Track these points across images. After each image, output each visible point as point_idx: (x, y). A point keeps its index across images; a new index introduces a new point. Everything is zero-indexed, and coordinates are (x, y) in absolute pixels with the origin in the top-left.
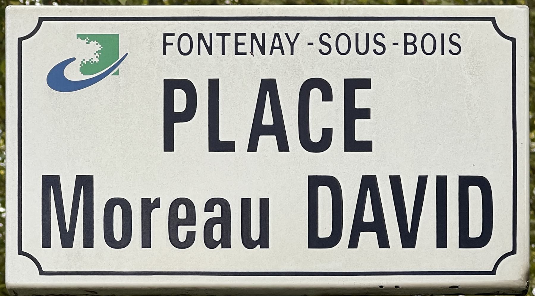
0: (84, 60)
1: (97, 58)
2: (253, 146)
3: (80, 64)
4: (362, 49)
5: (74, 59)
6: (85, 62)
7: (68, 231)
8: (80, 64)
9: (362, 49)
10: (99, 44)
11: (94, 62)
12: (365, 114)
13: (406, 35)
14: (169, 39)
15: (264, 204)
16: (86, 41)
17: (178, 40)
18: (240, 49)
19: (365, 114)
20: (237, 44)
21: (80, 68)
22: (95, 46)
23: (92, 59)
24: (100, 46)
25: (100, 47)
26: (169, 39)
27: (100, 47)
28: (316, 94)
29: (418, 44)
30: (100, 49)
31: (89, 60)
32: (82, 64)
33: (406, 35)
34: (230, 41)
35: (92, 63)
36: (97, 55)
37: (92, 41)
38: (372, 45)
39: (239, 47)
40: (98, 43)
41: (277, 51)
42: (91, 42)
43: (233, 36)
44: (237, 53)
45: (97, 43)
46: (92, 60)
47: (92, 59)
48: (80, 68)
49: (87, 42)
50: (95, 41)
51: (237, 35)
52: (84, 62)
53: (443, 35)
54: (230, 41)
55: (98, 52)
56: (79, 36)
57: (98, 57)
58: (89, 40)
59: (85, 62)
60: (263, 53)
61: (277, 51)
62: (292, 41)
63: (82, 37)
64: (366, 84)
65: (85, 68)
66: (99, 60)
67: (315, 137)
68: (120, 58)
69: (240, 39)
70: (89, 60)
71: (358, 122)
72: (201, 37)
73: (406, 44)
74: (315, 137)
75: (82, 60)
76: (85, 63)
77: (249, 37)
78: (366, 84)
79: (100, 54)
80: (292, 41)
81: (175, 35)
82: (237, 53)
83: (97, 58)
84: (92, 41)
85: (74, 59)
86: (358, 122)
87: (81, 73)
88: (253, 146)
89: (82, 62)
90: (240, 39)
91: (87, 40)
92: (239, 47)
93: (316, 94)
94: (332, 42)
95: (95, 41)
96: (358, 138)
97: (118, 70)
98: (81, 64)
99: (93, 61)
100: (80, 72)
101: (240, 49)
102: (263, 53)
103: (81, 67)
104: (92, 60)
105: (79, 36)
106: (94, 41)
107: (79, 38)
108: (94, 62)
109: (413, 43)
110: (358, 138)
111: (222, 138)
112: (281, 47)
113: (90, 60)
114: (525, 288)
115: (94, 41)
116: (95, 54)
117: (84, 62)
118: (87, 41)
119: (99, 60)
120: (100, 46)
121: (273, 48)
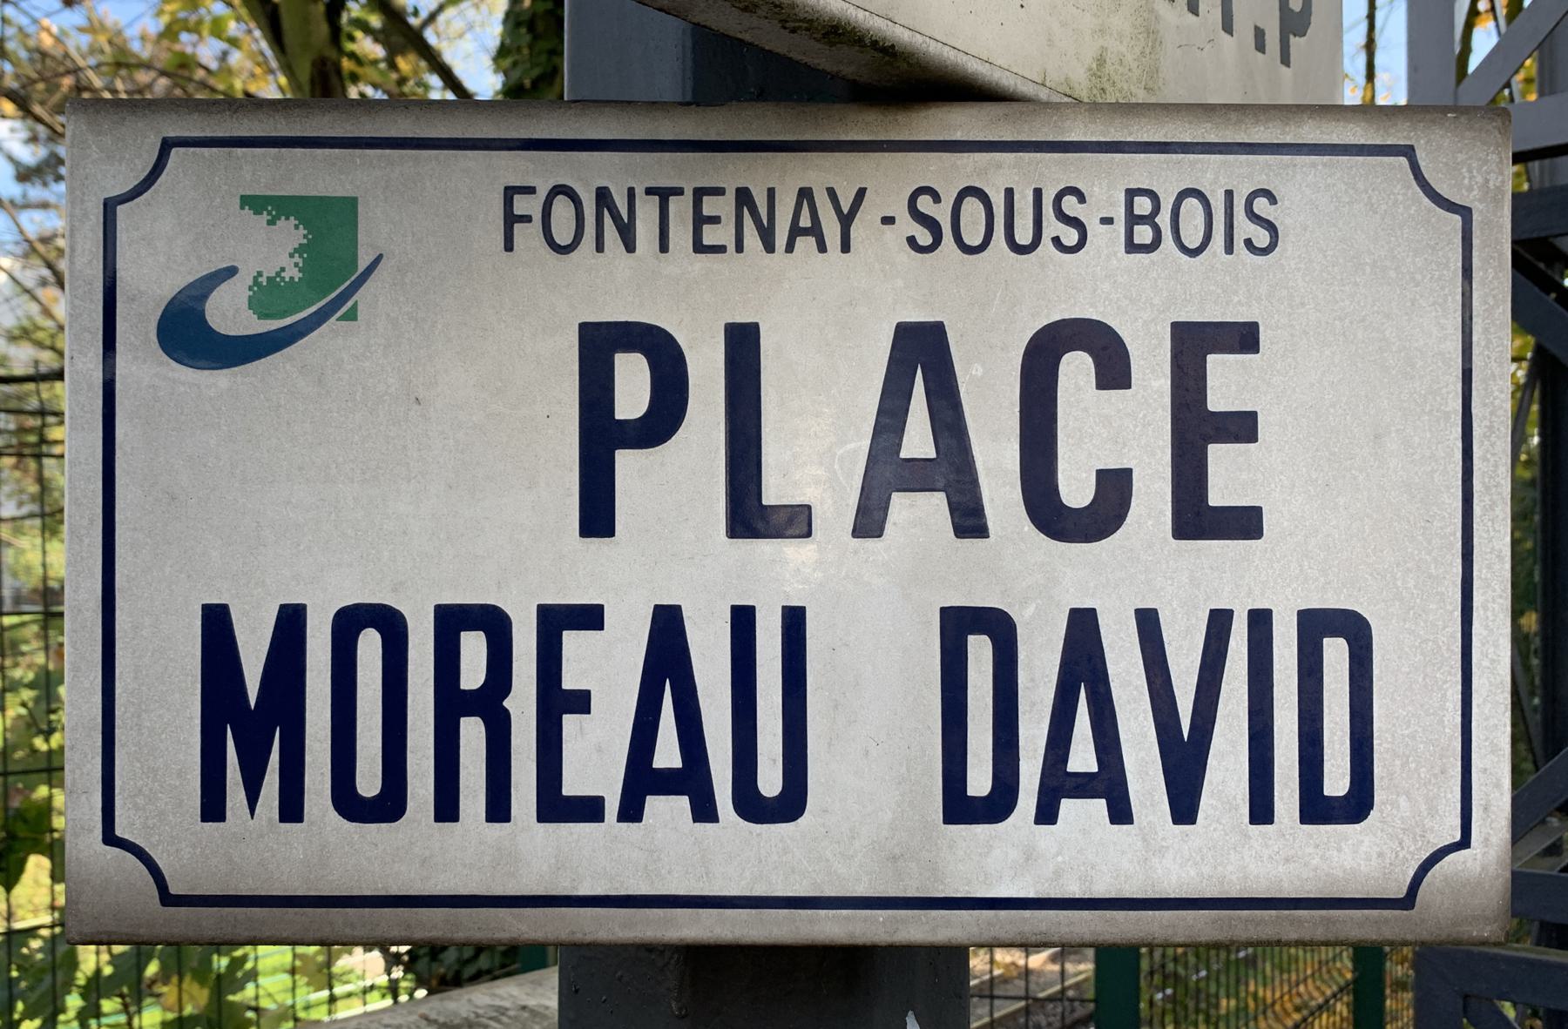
0: (260, 274)
1: (297, 269)
2: (869, 522)
3: (250, 287)
4: (1024, 236)
5: (231, 272)
6: (263, 280)
7: (253, 703)
8: (250, 287)
9: (1024, 236)
10: (301, 226)
11: (287, 279)
12: (1242, 427)
13: (1131, 194)
14: (521, 205)
15: (794, 621)
16: (265, 217)
17: (1416, 178)
18: (710, 236)
19: (1242, 427)
20: (700, 221)
21: (250, 297)
22: (290, 234)
23: (283, 269)
24: (306, 232)
25: (305, 237)
26: (521, 205)
27: (305, 237)
28: (1076, 369)
29: (1164, 220)
30: (305, 241)
31: (274, 275)
32: (254, 285)
33: (1131, 194)
34: (680, 208)
35: (282, 284)
36: (297, 259)
37: (283, 218)
38: (1052, 226)
39: (706, 228)
40: (300, 223)
41: (805, 244)
42: (279, 219)
43: (689, 194)
44: (699, 247)
45: (297, 222)
46: (283, 274)
47: (283, 269)
48: (250, 297)
49: (268, 221)
50: (292, 218)
51: (699, 193)
52: (260, 279)
53: (1229, 194)
54: (680, 208)
55: (300, 250)
56: (247, 201)
57: (301, 265)
58: (274, 213)
59: (263, 280)
60: (723, 249)
61: (805, 244)
62: (846, 211)
63: (253, 203)
64: (1244, 338)
65: (267, 295)
66: (301, 275)
67: (1076, 490)
68: (362, 265)
69: (710, 206)
70: (274, 275)
71: (1218, 455)
72: (603, 196)
73: (1133, 220)
74: (1076, 490)
75: (256, 274)
76: (265, 284)
77: (730, 196)
78: (1244, 338)
79: (305, 255)
80: (846, 211)
81: (771, 186)
82: (699, 247)
83: (297, 269)
84: (283, 218)
85: (231, 272)
86: (1218, 455)
87: (252, 311)
88: (869, 522)
89: (255, 279)
90: (710, 206)
91: (269, 213)
92: (706, 228)
93: (1076, 369)
94: (942, 214)
95: (292, 218)
96: (1217, 497)
97: (356, 302)
98: (251, 284)
99: (286, 275)
100: (250, 309)
101: (710, 236)
102: (769, 247)
103: (251, 293)
104: (283, 274)
105: (247, 201)
106: (287, 219)
107: (247, 207)
108: (287, 279)
109: (1150, 220)
110: (1217, 497)
111: (772, 494)
112: (816, 231)
113: (278, 274)
114: (1558, 814)
115: (287, 219)
116: (291, 256)
117: (260, 279)
118: (269, 217)
119: (301, 275)
120: (306, 232)
121: (796, 231)
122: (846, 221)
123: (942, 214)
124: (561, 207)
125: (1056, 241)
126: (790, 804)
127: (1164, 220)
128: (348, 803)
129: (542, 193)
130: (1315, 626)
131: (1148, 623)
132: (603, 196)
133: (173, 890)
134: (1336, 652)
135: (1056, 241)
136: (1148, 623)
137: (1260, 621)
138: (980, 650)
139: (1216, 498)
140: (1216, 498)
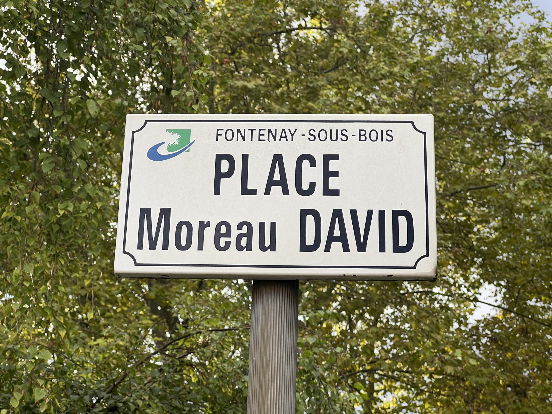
4: (334, 138)
9: (334, 138)
12: (336, 174)
14: (220, 132)
18: (262, 138)
19: (336, 174)
20: (260, 135)
28: (306, 163)
29: (367, 135)
38: (340, 136)
41: (283, 139)
43: (258, 131)
44: (259, 140)
61: (283, 139)
63: (169, 131)
64: (336, 157)
65: (170, 148)
67: (305, 186)
69: (262, 132)
72: (239, 131)
73: (360, 135)
74: (305, 186)
77: (267, 131)
78: (336, 157)
93: (306, 163)
94: (316, 134)
96: (331, 188)
101: (262, 138)
110: (331, 188)
111: (249, 187)
122: (292, 135)
123: (316, 134)
124: (229, 133)
125: (341, 139)
126: (272, 247)
127: (367, 135)
128: (179, 246)
129: (225, 131)
130: (396, 214)
131: (354, 213)
132: (239, 131)
133: (138, 262)
134: (402, 220)
135: (341, 139)
136: (354, 213)
137: (382, 214)
138: (310, 219)
139: (249, 187)
140: (249, 187)
